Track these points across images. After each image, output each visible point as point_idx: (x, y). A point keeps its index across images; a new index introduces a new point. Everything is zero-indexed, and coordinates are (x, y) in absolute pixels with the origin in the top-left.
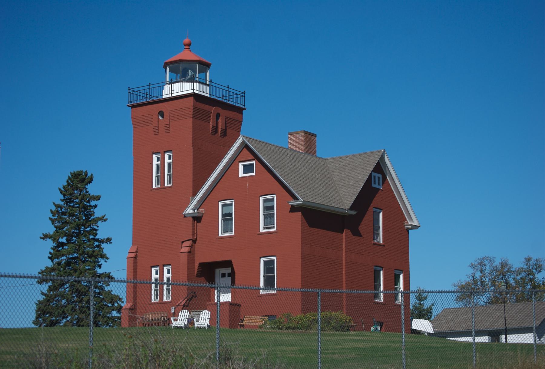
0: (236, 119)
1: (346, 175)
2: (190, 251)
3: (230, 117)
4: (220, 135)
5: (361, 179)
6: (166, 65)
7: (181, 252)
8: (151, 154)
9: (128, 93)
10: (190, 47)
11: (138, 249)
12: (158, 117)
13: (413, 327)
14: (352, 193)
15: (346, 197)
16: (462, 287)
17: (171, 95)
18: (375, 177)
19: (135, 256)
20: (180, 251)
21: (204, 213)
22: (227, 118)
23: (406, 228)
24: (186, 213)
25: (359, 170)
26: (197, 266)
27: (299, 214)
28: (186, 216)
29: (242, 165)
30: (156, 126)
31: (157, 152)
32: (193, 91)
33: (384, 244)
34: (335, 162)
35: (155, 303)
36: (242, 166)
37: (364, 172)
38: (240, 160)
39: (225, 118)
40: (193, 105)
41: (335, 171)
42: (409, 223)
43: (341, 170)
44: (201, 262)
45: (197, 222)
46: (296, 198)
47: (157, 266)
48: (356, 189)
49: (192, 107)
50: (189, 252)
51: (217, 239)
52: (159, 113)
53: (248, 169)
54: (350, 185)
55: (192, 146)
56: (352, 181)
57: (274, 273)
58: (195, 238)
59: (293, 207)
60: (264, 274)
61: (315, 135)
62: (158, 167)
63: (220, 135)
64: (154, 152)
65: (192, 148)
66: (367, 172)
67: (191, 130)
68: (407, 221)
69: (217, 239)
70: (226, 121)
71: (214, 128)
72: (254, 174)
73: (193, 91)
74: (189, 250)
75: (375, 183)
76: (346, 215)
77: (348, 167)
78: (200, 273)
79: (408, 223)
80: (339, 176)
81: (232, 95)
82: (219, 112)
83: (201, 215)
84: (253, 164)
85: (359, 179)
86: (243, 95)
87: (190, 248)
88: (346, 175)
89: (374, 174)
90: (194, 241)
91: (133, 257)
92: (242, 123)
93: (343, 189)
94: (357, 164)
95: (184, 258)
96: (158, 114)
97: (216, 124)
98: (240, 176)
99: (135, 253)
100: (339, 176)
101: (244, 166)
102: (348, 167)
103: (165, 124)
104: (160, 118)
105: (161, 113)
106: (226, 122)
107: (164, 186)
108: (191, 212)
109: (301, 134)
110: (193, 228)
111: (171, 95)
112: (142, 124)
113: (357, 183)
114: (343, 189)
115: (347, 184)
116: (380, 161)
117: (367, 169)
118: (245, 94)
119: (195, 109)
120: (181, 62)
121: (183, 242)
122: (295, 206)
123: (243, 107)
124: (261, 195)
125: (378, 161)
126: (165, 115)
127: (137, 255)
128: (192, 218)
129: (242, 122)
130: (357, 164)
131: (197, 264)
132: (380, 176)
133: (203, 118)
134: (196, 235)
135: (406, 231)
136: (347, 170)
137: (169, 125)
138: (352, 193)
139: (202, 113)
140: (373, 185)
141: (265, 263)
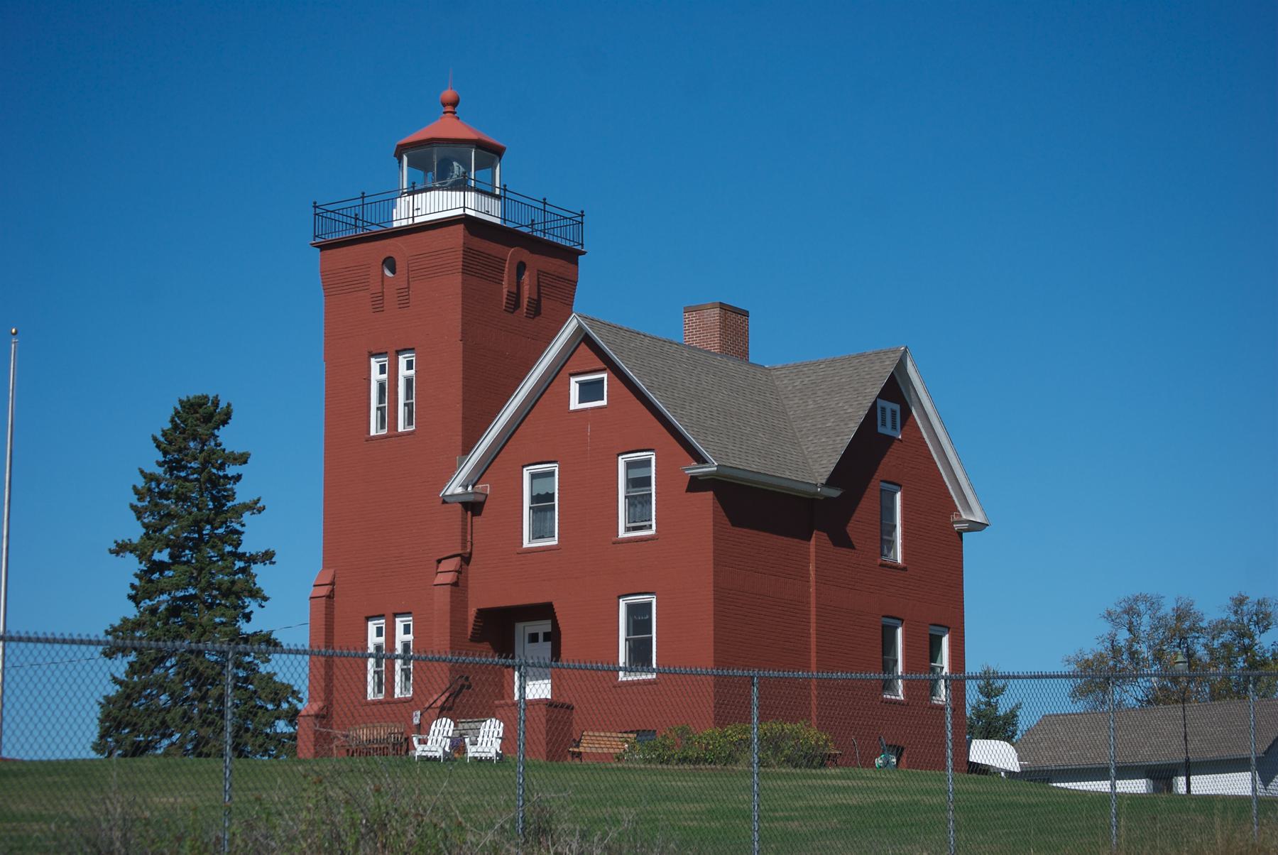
1: (816, 406)
7: (435, 583)
8: (367, 356)
12: (383, 271)
17: (413, 220)
18: (883, 409)
19: (328, 594)
20: (433, 582)
21: (488, 492)
23: (956, 529)
24: (448, 493)
25: (847, 393)
26: (473, 617)
32: (464, 211)
35: (375, 703)
36: (578, 385)
39: (538, 275)
40: (464, 244)
42: (964, 517)
45: (473, 515)
46: (701, 460)
48: (840, 438)
50: (455, 584)
51: (518, 554)
53: (590, 390)
54: (827, 429)
55: (460, 338)
56: (832, 420)
58: (469, 550)
59: (694, 479)
61: (745, 314)
62: (382, 386)
64: (374, 352)
66: (867, 398)
68: (959, 512)
69: (518, 554)
70: (540, 280)
72: (604, 403)
74: (455, 580)
75: (884, 424)
76: (816, 497)
77: (822, 387)
79: (961, 516)
82: (523, 260)
83: (481, 498)
84: (602, 380)
85: (848, 415)
86: (579, 219)
88: (816, 406)
89: (881, 403)
90: (466, 559)
94: (843, 380)
95: (443, 598)
98: (572, 407)
102: (822, 387)
103: (398, 287)
104: (388, 273)
105: (390, 263)
106: (539, 282)
107: (396, 432)
108: (460, 490)
111: (413, 220)
113: (842, 424)
115: (820, 426)
119: (468, 252)
121: (439, 561)
123: (579, 248)
126: (400, 266)
127: (333, 590)
128: (460, 505)
129: (576, 282)
130: (843, 380)
131: (472, 613)
132: (897, 407)
134: (469, 544)
136: (820, 393)
140: (881, 430)
141: (631, 608)
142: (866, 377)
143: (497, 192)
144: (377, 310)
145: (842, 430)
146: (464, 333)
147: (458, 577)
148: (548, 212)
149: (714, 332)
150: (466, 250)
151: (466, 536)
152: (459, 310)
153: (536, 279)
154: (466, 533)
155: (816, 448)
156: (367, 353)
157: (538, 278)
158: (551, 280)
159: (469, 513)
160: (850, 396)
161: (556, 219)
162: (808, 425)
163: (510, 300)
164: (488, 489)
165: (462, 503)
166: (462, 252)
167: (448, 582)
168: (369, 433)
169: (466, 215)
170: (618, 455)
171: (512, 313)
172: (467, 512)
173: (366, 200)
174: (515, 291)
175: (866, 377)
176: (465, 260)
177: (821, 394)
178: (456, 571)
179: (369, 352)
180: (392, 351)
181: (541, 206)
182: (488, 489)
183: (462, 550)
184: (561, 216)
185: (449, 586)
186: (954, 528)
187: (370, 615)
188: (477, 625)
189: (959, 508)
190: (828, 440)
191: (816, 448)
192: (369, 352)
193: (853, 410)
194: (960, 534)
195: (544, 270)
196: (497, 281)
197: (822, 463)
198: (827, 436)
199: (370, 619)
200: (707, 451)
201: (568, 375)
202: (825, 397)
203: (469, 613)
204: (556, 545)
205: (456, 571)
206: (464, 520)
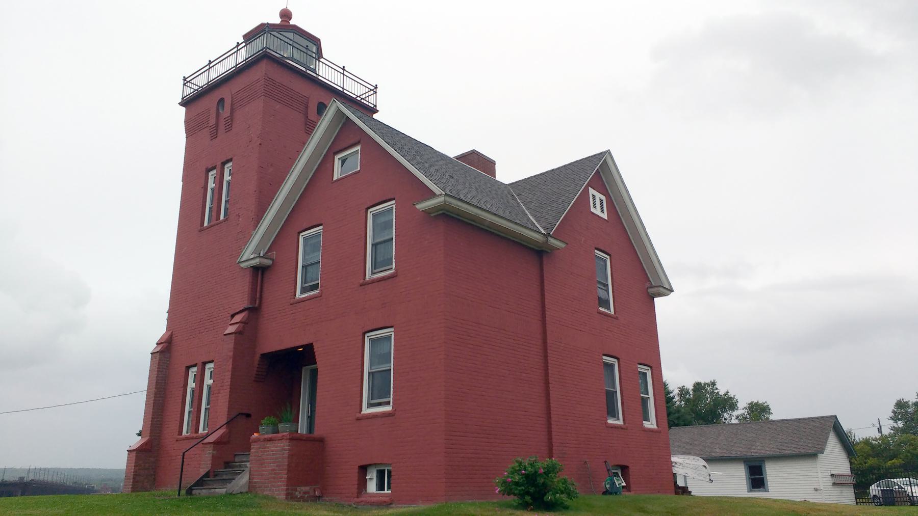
11: (173, 336)
21: (274, 258)
47: (195, 365)
51: (291, 304)
59: (427, 212)
69: (291, 304)
89: (592, 191)
121: (233, 316)
128: (251, 269)
131: (258, 357)
140: (593, 210)
147: (244, 327)
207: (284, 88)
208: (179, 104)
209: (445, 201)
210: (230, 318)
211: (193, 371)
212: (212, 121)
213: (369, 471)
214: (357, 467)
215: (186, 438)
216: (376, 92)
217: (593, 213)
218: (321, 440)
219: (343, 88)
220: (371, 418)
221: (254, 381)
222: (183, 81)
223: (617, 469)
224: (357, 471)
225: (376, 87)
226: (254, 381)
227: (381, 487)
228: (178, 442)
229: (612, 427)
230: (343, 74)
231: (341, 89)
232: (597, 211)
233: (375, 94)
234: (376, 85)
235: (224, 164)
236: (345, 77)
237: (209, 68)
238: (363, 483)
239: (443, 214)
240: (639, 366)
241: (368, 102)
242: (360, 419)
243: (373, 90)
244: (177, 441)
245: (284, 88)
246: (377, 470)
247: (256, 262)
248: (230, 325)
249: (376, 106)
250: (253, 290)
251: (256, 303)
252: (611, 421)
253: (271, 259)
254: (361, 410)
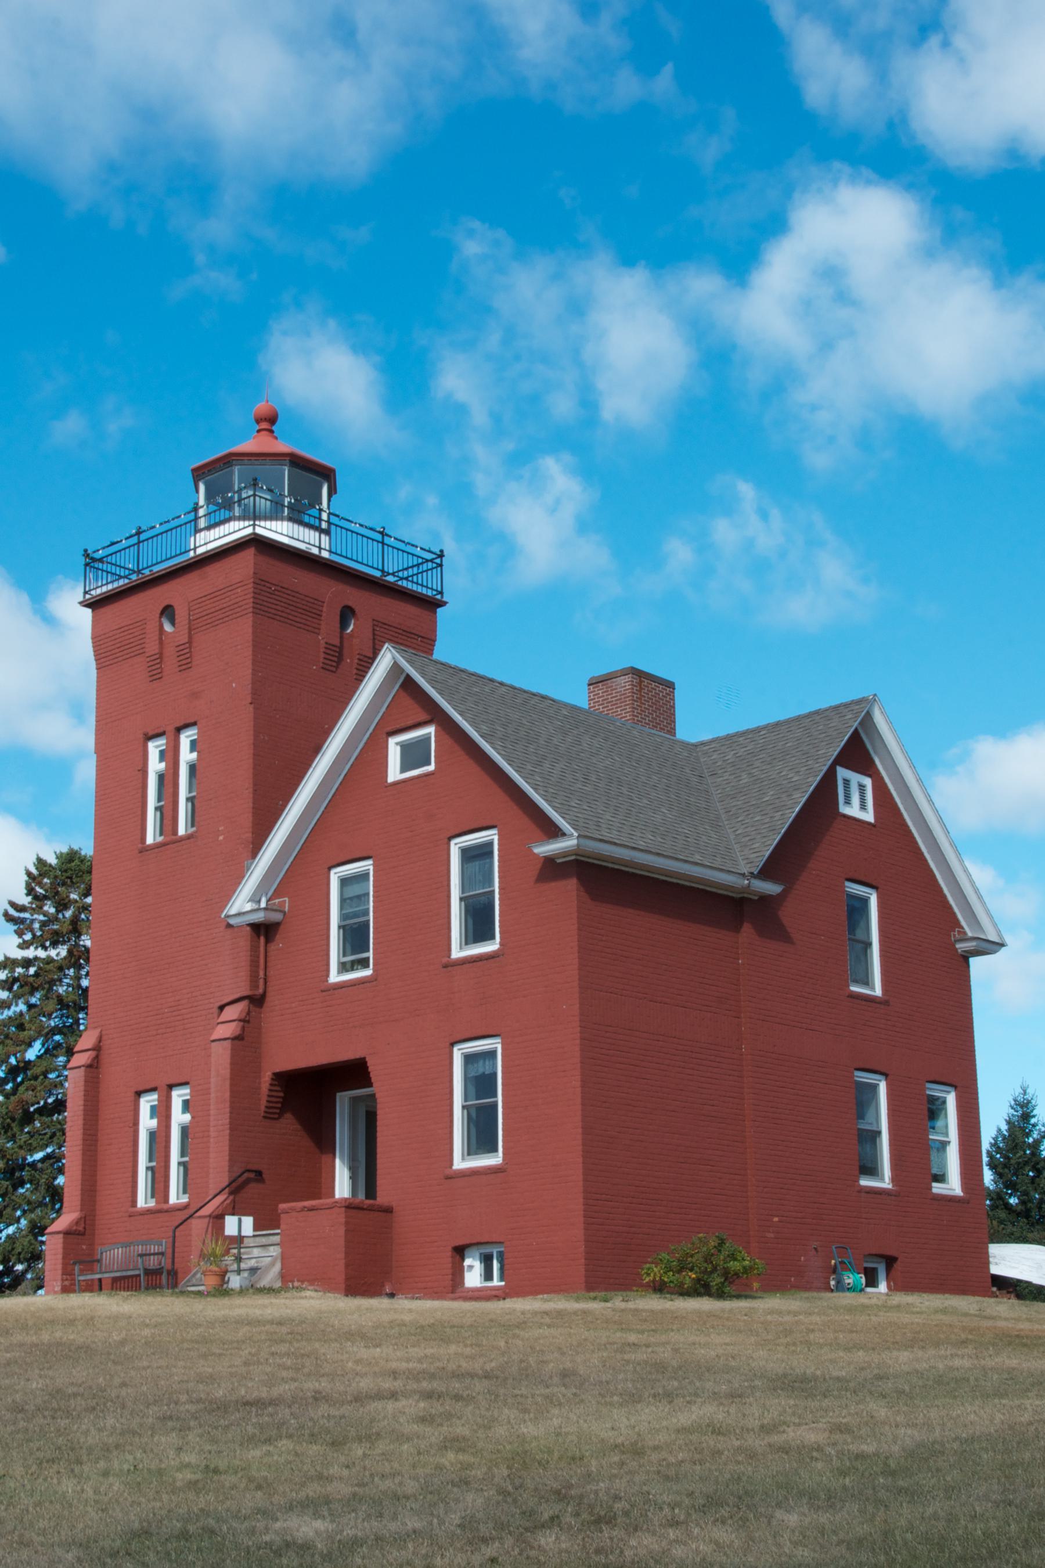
0: (414, 631)
1: (751, 779)
2: (239, 1035)
3: (390, 623)
4: (324, 653)
5: (797, 783)
6: (199, 473)
7: (212, 1038)
8: (142, 740)
9: (83, 567)
10: (274, 428)
11: (104, 1038)
12: (161, 626)
13: (997, 1269)
14: (767, 825)
15: (748, 838)
16: (998, 283)
17: (195, 552)
18: (847, 782)
19: (89, 1062)
20: (211, 1034)
21: (287, 909)
22: (380, 625)
23: (959, 951)
24: (233, 911)
25: (793, 759)
26: (267, 1085)
27: (571, 885)
28: (232, 921)
29: (397, 744)
30: (153, 653)
31: (156, 731)
32: (254, 529)
33: (886, 998)
34: (723, 748)
35: (149, 1212)
36: (398, 748)
37: (810, 763)
38: (389, 729)
39: (374, 625)
40: (254, 573)
41: (723, 771)
42: (970, 934)
43: (738, 767)
44: (278, 1071)
45: (268, 941)
46: (553, 832)
47: (153, 1090)
48: (780, 813)
49: (252, 580)
50: (237, 1038)
51: (322, 991)
52: (162, 613)
53: (413, 755)
54: (763, 805)
55: (249, 700)
56: (772, 793)
57: (495, 1095)
58: (261, 991)
59: (549, 862)
60: (466, 1100)
61: (670, 685)
62: (161, 777)
63: (356, 674)
64: (151, 733)
65: (252, 706)
66: (820, 760)
67: (249, 652)
68: (963, 928)
69: (322, 991)
70: (376, 632)
71: (335, 651)
72: (431, 768)
73: (254, 529)
74: (238, 1032)
75: (848, 802)
76: (746, 895)
77: (761, 756)
78: (279, 1105)
79: (965, 933)
80: (732, 784)
81: (410, 565)
82: (350, 604)
83: (277, 917)
84: (426, 739)
85: (793, 784)
86: (438, 561)
87: (242, 1023)
88: (751, 779)
89: (842, 773)
90: (257, 1001)
91: (83, 1066)
92: (434, 646)
93: (739, 819)
94: (788, 745)
95: (221, 1057)
96: (160, 617)
97: (339, 640)
98: (391, 779)
99: (89, 1053)
100: (732, 784)
101: (405, 747)
102: (761, 756)
103: (177, 644)
104: (168, 627)
105: (168, 611)
106: (374, 634)
107: (174, 837)
108: (248, 907)
109: (622, 678)
110: (252, 961)
111: (195, 552)
112: (118, 655)
113: (784, 795)
114: (739, 819)
115: (754, 803)
116: (861, 731)
117: (820, 752)
118: (444, 558)
119: (260, 583)
120: (234, 462)
121: (222, 1008)
122: (559, 861)
123: (439, 597)
124: (453, 834)
125: (856, 730)
126: (181, 613)
127: (97, 1057)
128: (248, 928)
129: (435, 641)
130: (788, 745)
131: (266, 1078)
132: (868, 782)
133: (291, 617)
134: (261, 982)
135: (961, 959)
136: (757, 764)
137: (187, 645)
138: (767, 825)
139: (288, 602)
140: (845, 810)
141: (469, 1059)
142: (820, 736)
143: (324, 525)
144: (155, 677)
145: (783, 804)
146: (255, 693)
147: (243, 1028)
148: (388, 546)
149: (625, 705)
150: (259, 582)
151: (258, 972)
152: (249, 663)
153: (371, 630)
154: (258, 966)
155: (747, 830)
156: (141, 736)
157: (374, 630)
158: (394, 634)
159: (262, 939)
160: (797, 761)
161: (415, 563)
162: (739, 803)
163: (257, 608)
164: (287, 905)
165: (249, 925)
166: (252, 585)
167: (228, 1036)
168: (449, 955)
169: (254, 534)
170: (450, 838)
171: (334, 672)
172: (259, 937)
173: (143, 537)
174: (339, 645)
175: (820, 736)
176: (256, 596)
177: (759, 765)
178: (240, 1020)
179: (145, 735)
180: (170, 729)
181: (379, 537)
182: (287, 905)
183: (251, 990)
184: (423, 558)
185: (230, 1041)
186: (956, 950)
187: (141, 1088)
188: (272, 1096)
189: (963, 923)
190: (764, 817)
191: (747, 830)
192: (145, 735)
193: (801, 777)
194: (965, 958)
195: (384, 621)
196: (310, 628)
197: (754, 846)
198: (762, 813)
199: (142, 1095)
200: (563, 817)
201: (384, 736)
202: (764, 768)
203: (263, 1080)
204: (372, 975)
205: (240, 1020)
206: (254, 949)
207: (284, 593)
208: (80, 603)
209: (578, 845)
210: (216, 1011)
211: (147, 1103)
212: (152, 647)
213: (467, 1253)
214: (450, 1248)
215: (148, 1211)
216: (441, 565)
217: (845, 816)
218: (388, 1210)
219: (383, 571)
220: (469, 1176)
221: (265, 1117)
222: (83, 558)
223: (877, 1262)
224: (449, 1254)
225: (441, 555)
226: (265, 1117)
227: (488, 1275)
228: (132, 1218)
229: (868, 1193)
230: (383, 543)
231: (378, 574)
232: (853, 810)
233: (87, 589)
234: (442, 551)
235: (179, 730)
236: (386, 547)
237: (139, 542)
238: (458, 1273)
239: (576, 860)
240: (928, 1085)
241: (427, 587)
242: (317, 1209)
243: (432, 561)
244: (130, 1216)
245: (284, 593)
246: (481, 1254)
247: (259, 917)
248: (218, 1023)
249: (441, 593)
250: (254, 963)
251: (257, 987)
252: (865, 1182)
253: (281, 911)
254: (452, 1164)
